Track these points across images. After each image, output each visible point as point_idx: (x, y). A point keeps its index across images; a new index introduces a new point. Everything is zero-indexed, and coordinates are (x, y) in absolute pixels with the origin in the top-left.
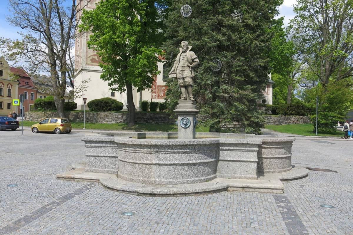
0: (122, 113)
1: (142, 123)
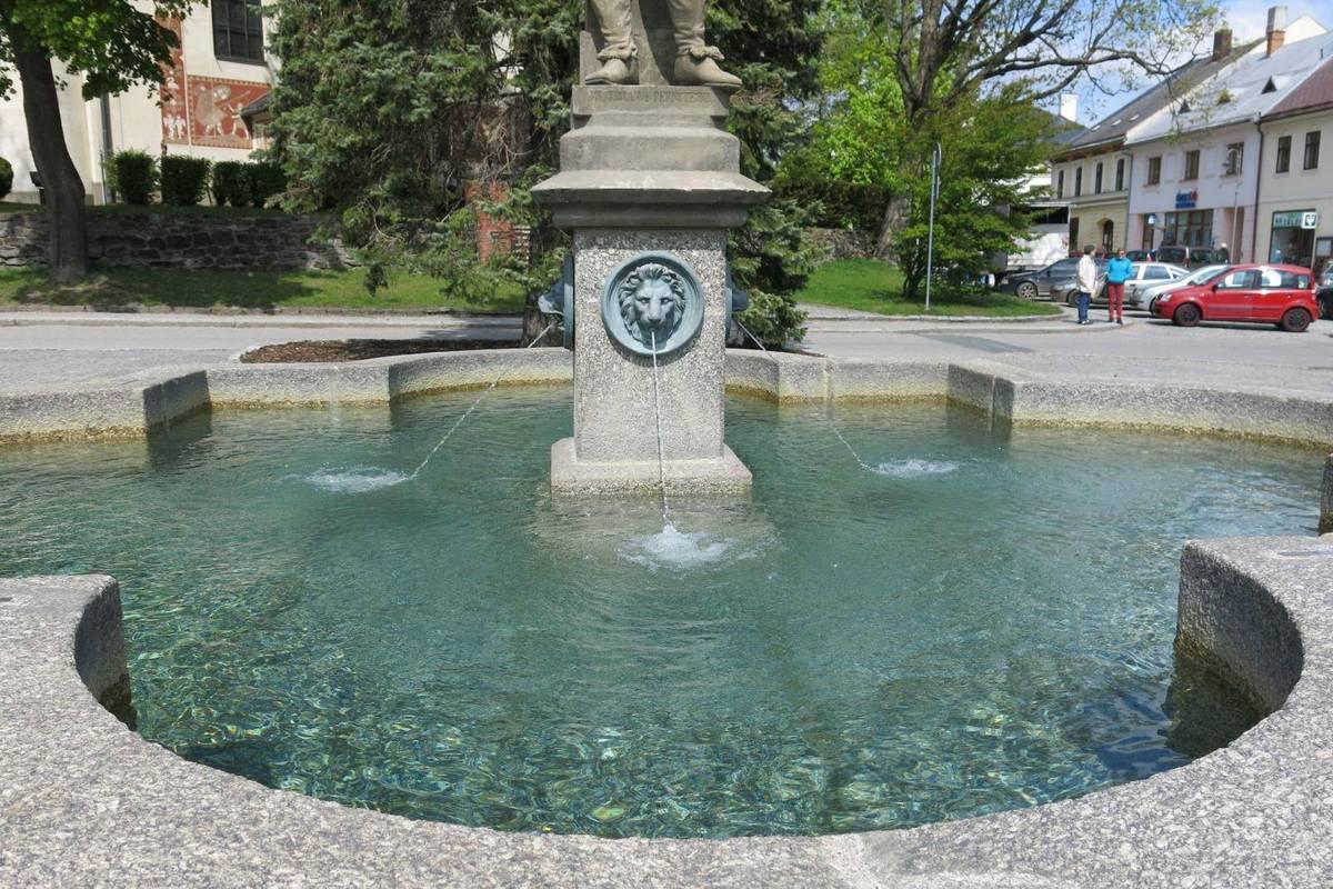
0: (9, 215)
1: (127, 267)
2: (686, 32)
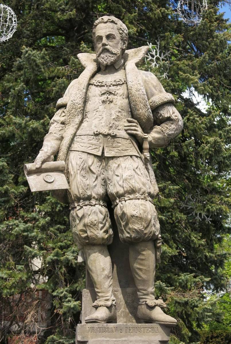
2: (144, 292)
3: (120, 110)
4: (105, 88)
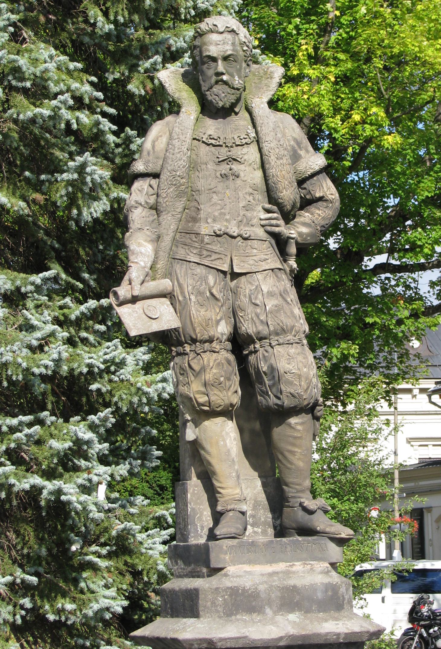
3: (251, 190)
4: (223, 153)
